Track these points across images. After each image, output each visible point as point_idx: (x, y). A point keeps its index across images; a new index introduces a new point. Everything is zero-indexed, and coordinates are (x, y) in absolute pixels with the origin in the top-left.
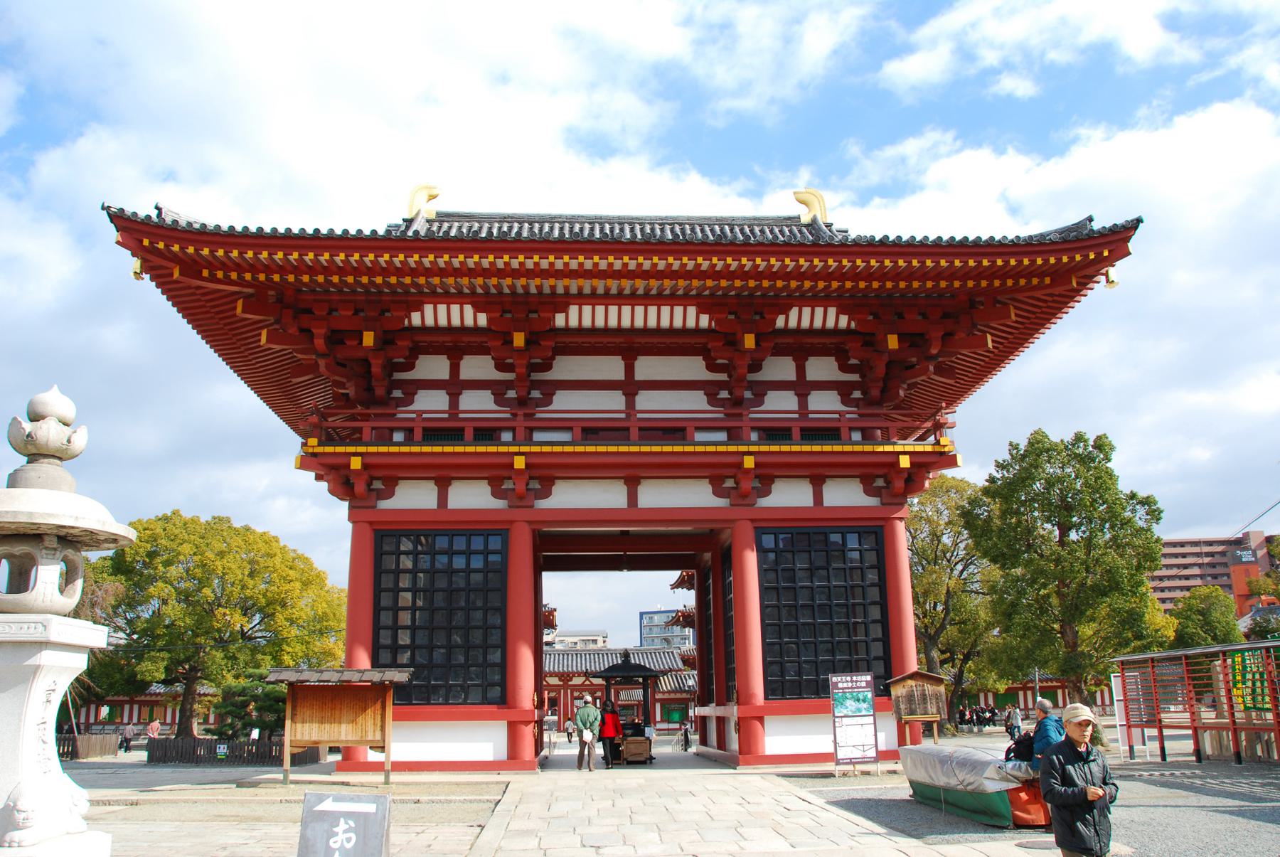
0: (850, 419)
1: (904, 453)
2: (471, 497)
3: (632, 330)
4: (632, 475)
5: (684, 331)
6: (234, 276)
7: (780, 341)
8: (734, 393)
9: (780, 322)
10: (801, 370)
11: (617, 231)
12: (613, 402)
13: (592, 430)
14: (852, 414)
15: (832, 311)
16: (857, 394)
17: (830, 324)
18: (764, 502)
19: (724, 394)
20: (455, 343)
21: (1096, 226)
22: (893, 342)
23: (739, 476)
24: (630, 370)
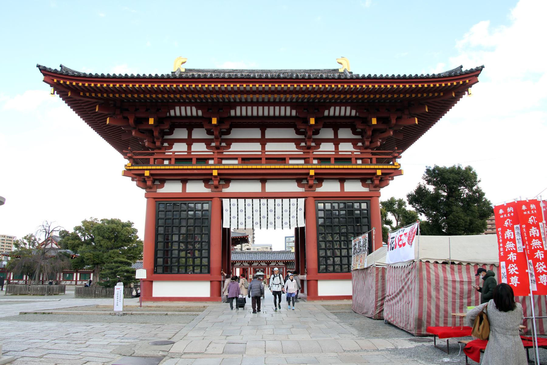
0: (356, 155)
1: (379, 169)
3: (263, 117)
5: (285, 117)
6: (88, 94)
7: (235, 121)
9: (326, 113)
10: (190, 134)
12: (256, 147)
14: (357, 153)
15: (348, 109)
17: (348, 114)
19: (360, 144)
21: (463, 70)
22: (374, 121)
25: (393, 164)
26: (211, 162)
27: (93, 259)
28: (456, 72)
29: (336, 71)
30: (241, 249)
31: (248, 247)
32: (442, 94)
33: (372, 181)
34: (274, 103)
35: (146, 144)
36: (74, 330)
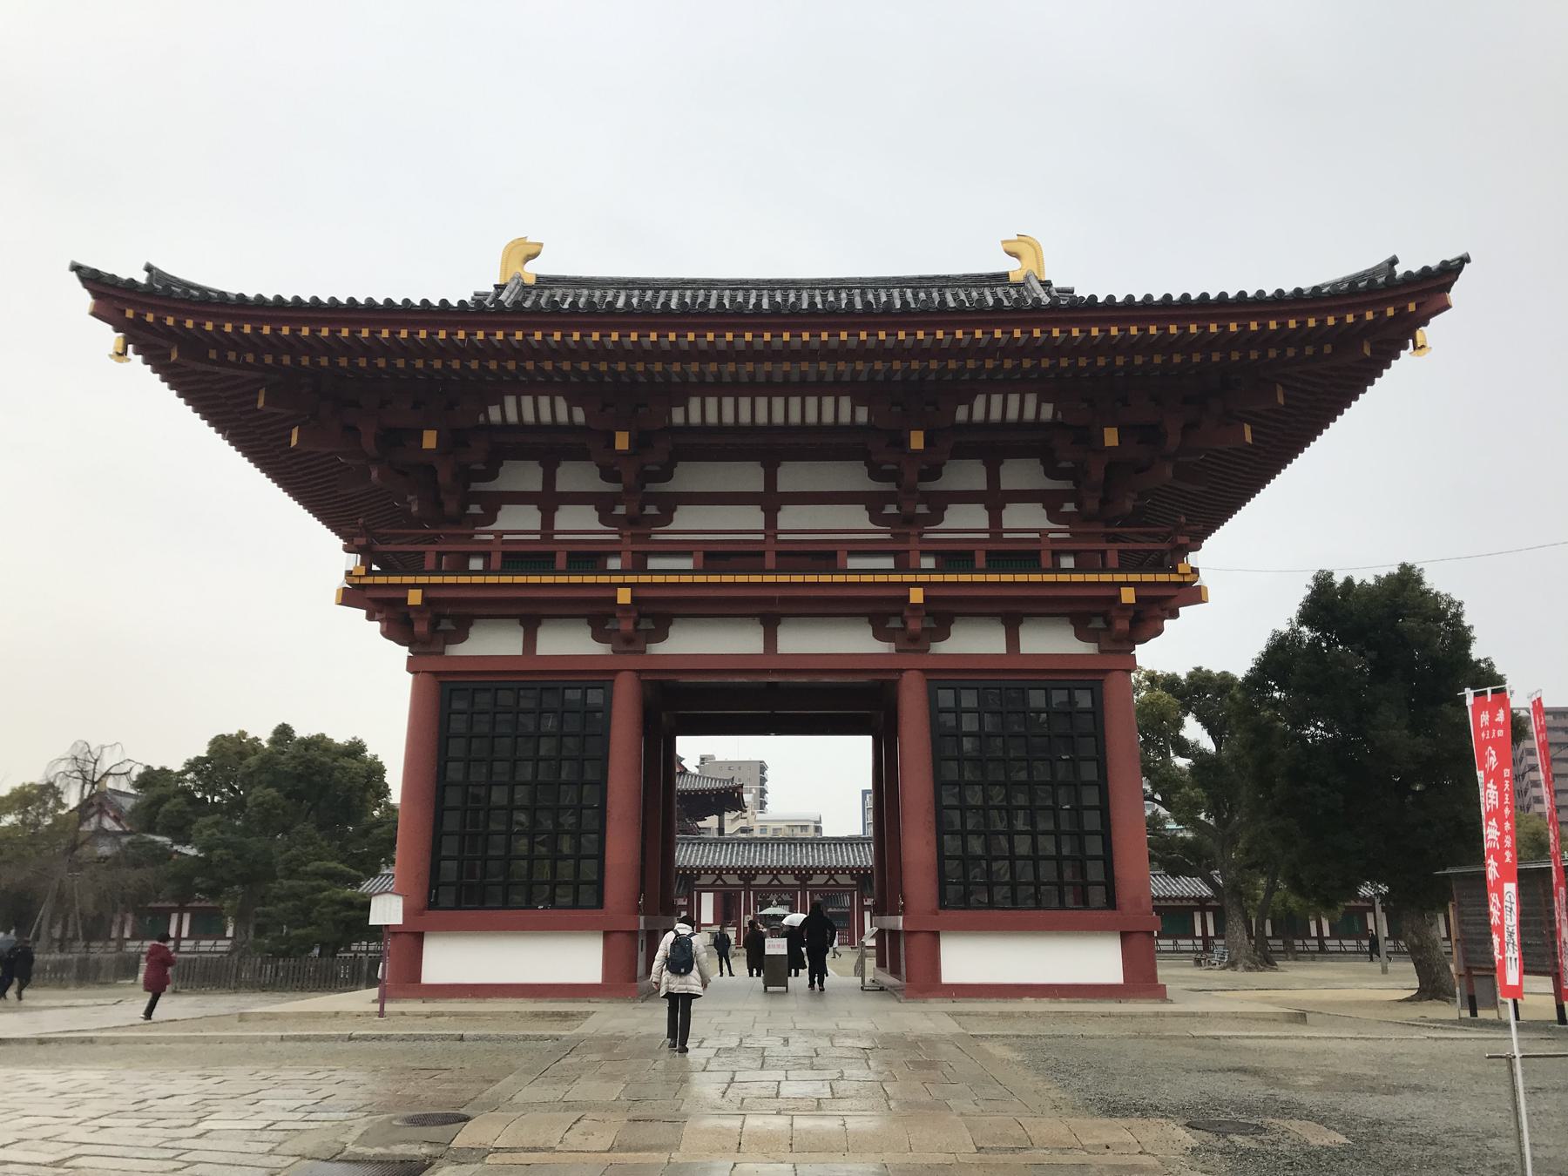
0: (1053, 540)
1: (1128, 584)
2: (567, 642)
3: (770, 428)
4: (770, 613)
5: (836, 428)
6: (232, 356)
8: (906, 507)
9: (961, 414)
11: (884, 299)
12: (749, 519)
13: (716, 556)
16: (1069, 507)
18: (658, 649)
20: (549, 447)
21: (1400, 270)
22: (1111, 438)
23: (906, 613)
24: (771, 480)
25: (1175, 570)
26: (614, 563)
27: (229, 872)
28: (1372, 281)
29: (1000, 279)
30: (721, 830)
31: (742, 823)
32: (1328, 349)
33: (1109, 623)
34: (803, 388)
35: (414, 508)
36: (165, 1089)
